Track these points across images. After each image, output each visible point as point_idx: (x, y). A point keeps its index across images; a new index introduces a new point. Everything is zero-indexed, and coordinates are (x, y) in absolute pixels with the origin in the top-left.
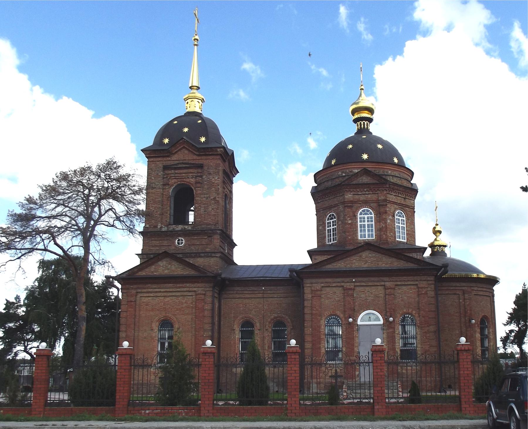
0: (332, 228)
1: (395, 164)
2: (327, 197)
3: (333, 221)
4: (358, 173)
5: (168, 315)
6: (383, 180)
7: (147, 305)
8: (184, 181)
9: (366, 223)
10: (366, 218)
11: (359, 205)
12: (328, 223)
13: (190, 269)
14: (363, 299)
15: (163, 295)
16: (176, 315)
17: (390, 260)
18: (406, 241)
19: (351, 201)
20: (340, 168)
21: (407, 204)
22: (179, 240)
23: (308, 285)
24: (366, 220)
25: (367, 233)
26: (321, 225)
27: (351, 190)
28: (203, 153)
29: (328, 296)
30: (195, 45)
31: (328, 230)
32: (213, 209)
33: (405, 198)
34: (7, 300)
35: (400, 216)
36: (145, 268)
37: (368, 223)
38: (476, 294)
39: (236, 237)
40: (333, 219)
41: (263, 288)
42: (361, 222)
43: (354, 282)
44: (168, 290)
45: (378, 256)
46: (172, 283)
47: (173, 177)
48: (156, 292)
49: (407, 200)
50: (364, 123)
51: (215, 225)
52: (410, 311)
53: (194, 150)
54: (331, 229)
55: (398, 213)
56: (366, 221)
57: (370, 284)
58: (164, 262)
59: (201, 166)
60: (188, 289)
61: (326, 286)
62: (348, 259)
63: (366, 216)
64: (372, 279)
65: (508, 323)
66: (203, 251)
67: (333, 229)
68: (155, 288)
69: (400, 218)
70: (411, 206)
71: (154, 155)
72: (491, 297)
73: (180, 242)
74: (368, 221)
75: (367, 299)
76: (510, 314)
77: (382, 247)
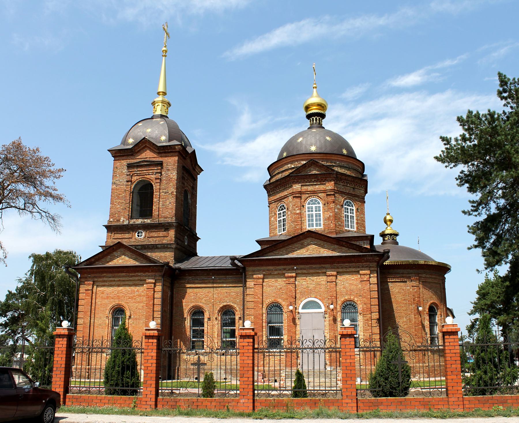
0: (282, 218)
1: (343, 155)
2: (278, 189)
3: (283, 212)
4: (305, 163)
5: (121, 303)
6: (330, 171)
7: (103, 293)
8: (145, 178)
9: (314, 213)
10: (314, 208)
11: (307, 195)
12: (279, 214)
13: (142, 259)
14: (305, 287)
15: (117, 284)
16: (128, 303)
17: (332, 247)
18: (355, 230)
19: (299, 192)
20: (289, 161)
21: (356, 194)
22: (139, 233)
23: (250, 273)
24: (314, 209)
25: (314, 222)
26: (273, 216)
27: (300, 181)
28: (163, 151)
29: (270, 284)
30: (163, 56)
31: (279, 221)
32: (170, 203)
33: (354, 188)
34: (8, 291)
35: (348, 205)
36: (102, 259)
37: (316, 213)
38: (424, 281)
39: (199, 232)
40: (282, 209)
41: (213, 277)
42: (309, 211)
43: (295, 270)
44: (121, 279)
45: (319, 243)
46: (125, 273)
47: (136, 174)
48: (111, 281)
49: (356, 190)
50: (316, 118)
51: (171, 218)
52: (352, 298)
53: (155, 148)
54: (281, 220)
55: (347, 202)
56: (314, 210)
57: (311, 271)
58: (119, 252)
59: (161, 164)
60: (139, 278)
61: (267, 274)
62: (290, 246)
63: (314, 206)
64: (314, 266)
65: (472, 313)
66: (161, 243)
67: (283, 219)
68: (110, 277)
69: (349, 208)
70: (361, 196)
71: (119, 155)
72: (442, 284)
73: (140, 234)
74: (316, 211)
75: (308, 287)
76: (475, 303)
77: (330, 236)
